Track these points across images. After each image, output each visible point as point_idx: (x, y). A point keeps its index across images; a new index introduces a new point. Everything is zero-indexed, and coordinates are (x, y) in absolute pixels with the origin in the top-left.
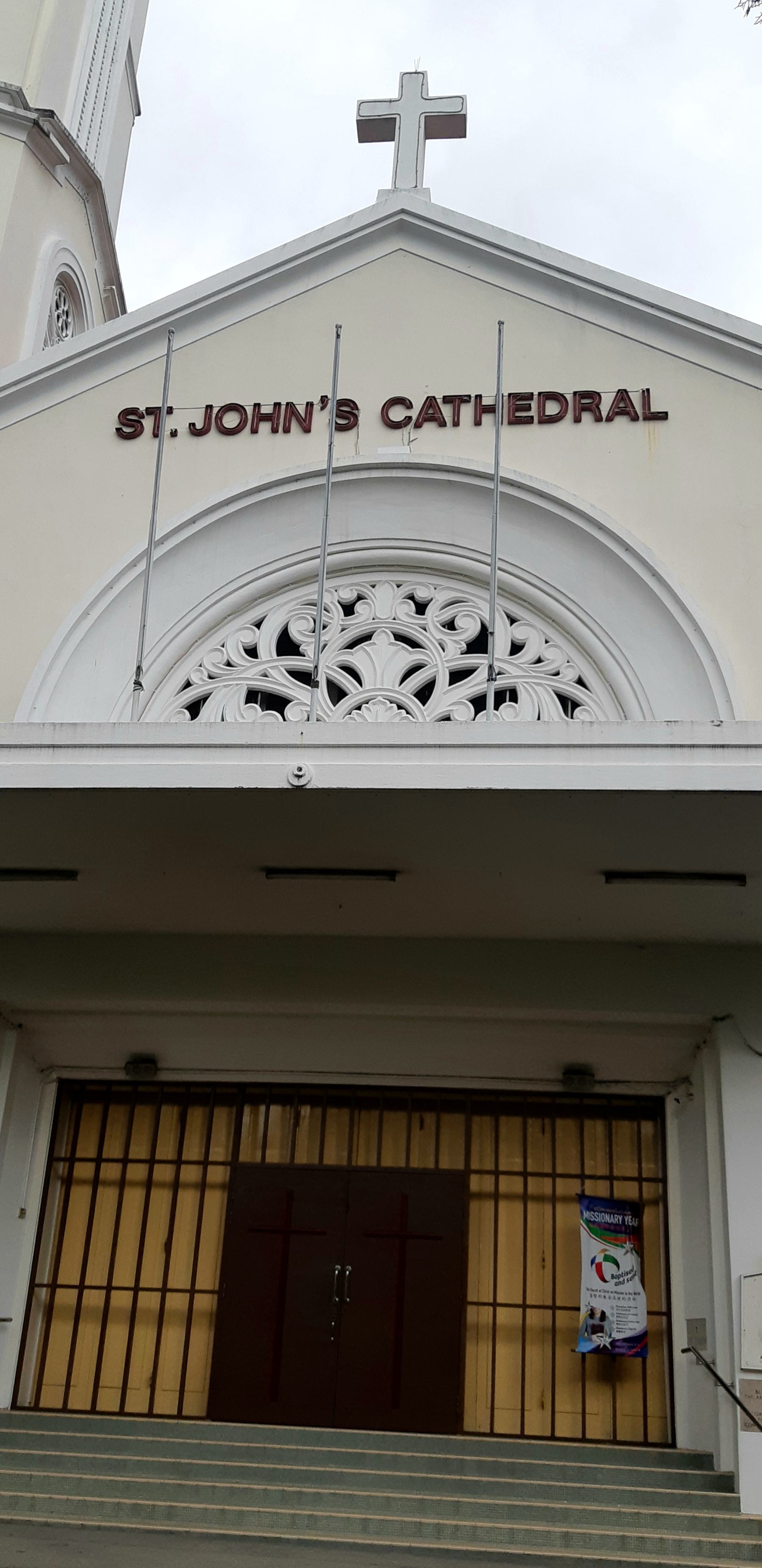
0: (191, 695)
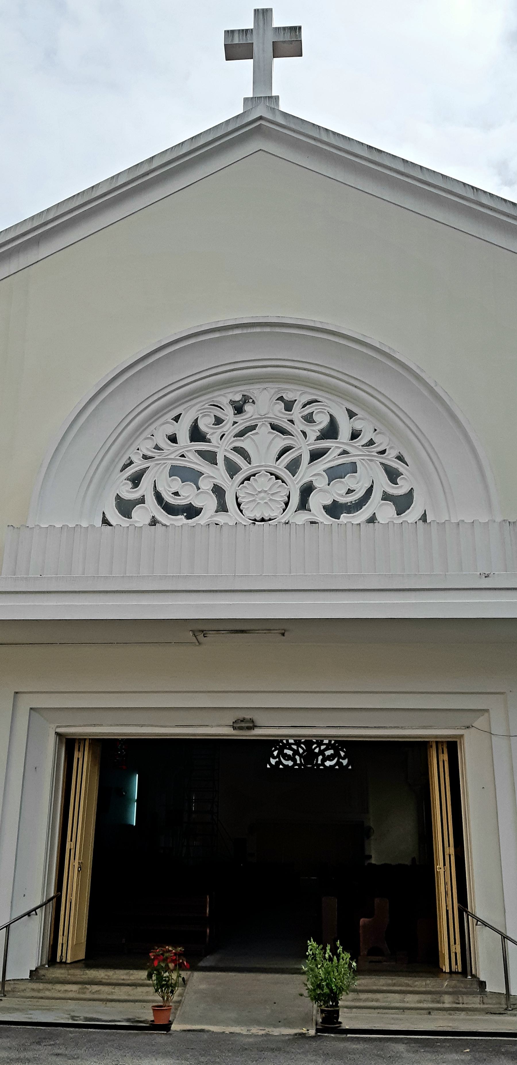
0: (131, 471)
